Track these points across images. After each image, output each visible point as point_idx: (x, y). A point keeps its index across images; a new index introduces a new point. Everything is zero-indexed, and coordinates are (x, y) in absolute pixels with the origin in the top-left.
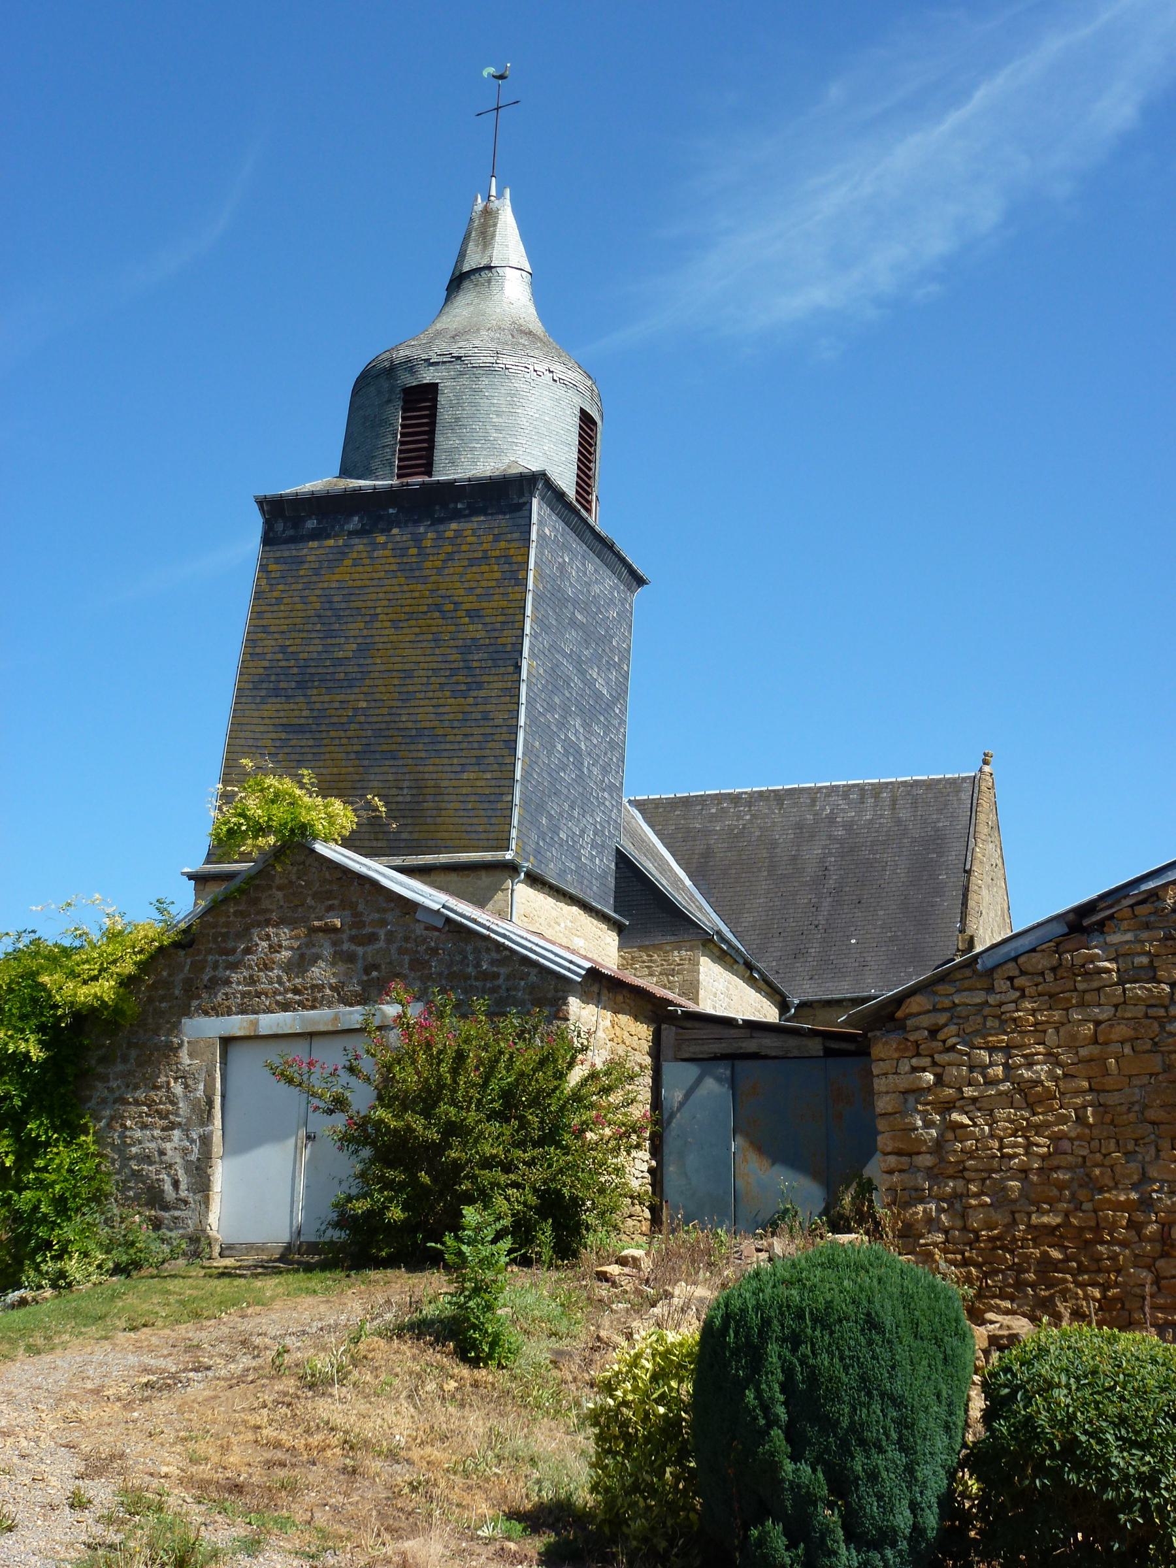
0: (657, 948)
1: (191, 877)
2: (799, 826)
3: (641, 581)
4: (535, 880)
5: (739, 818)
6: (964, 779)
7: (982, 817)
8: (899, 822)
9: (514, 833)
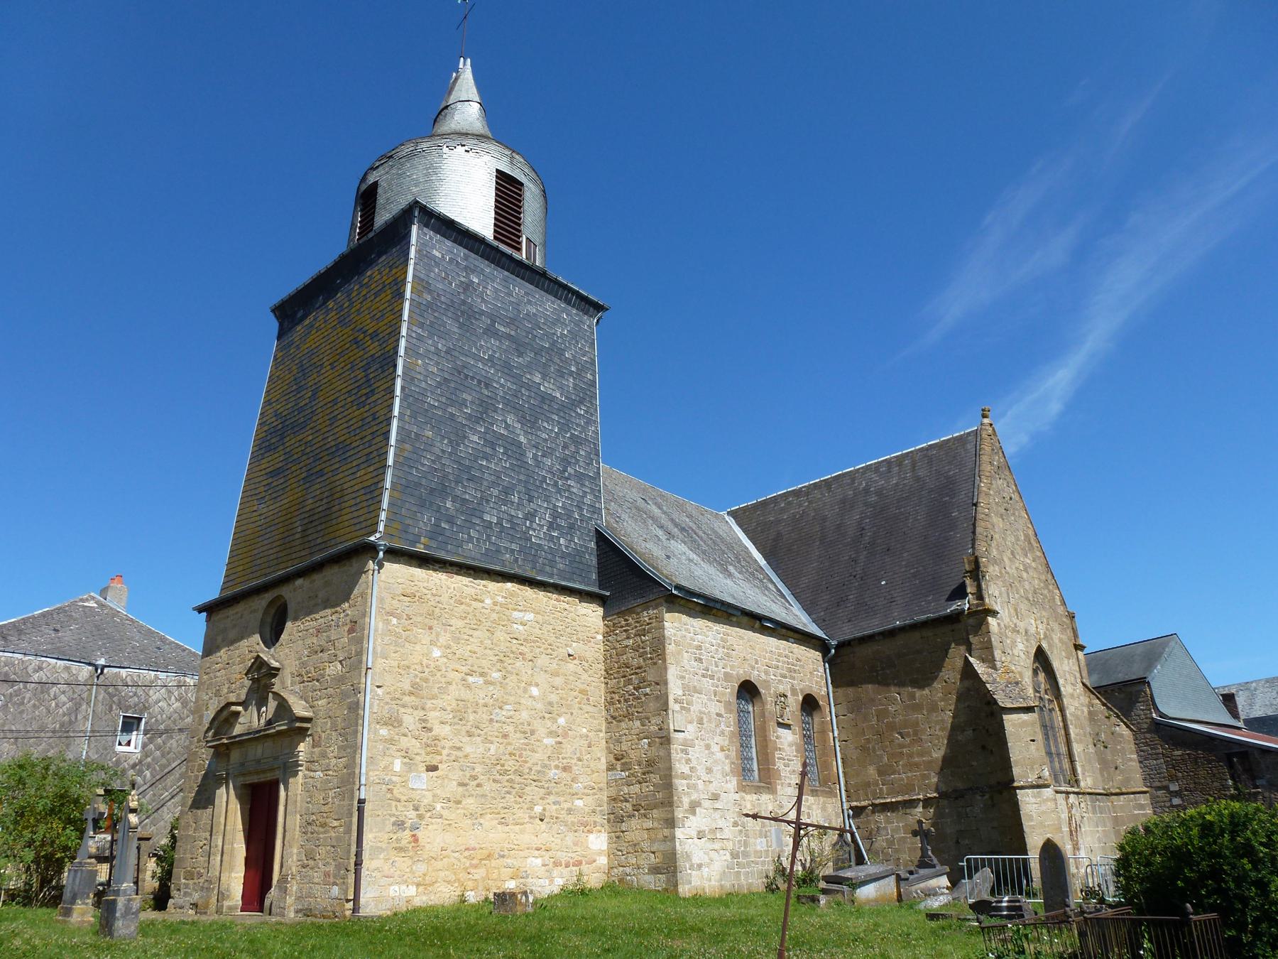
0: (630, 611)
1: (200, 610)
2: (843, 501)
3: (598, 308)
4: (395, 554)
5: (800, 505)
6: (969, 434)
7: (985, 458)
8: (918, 479)
9: (383, 516)
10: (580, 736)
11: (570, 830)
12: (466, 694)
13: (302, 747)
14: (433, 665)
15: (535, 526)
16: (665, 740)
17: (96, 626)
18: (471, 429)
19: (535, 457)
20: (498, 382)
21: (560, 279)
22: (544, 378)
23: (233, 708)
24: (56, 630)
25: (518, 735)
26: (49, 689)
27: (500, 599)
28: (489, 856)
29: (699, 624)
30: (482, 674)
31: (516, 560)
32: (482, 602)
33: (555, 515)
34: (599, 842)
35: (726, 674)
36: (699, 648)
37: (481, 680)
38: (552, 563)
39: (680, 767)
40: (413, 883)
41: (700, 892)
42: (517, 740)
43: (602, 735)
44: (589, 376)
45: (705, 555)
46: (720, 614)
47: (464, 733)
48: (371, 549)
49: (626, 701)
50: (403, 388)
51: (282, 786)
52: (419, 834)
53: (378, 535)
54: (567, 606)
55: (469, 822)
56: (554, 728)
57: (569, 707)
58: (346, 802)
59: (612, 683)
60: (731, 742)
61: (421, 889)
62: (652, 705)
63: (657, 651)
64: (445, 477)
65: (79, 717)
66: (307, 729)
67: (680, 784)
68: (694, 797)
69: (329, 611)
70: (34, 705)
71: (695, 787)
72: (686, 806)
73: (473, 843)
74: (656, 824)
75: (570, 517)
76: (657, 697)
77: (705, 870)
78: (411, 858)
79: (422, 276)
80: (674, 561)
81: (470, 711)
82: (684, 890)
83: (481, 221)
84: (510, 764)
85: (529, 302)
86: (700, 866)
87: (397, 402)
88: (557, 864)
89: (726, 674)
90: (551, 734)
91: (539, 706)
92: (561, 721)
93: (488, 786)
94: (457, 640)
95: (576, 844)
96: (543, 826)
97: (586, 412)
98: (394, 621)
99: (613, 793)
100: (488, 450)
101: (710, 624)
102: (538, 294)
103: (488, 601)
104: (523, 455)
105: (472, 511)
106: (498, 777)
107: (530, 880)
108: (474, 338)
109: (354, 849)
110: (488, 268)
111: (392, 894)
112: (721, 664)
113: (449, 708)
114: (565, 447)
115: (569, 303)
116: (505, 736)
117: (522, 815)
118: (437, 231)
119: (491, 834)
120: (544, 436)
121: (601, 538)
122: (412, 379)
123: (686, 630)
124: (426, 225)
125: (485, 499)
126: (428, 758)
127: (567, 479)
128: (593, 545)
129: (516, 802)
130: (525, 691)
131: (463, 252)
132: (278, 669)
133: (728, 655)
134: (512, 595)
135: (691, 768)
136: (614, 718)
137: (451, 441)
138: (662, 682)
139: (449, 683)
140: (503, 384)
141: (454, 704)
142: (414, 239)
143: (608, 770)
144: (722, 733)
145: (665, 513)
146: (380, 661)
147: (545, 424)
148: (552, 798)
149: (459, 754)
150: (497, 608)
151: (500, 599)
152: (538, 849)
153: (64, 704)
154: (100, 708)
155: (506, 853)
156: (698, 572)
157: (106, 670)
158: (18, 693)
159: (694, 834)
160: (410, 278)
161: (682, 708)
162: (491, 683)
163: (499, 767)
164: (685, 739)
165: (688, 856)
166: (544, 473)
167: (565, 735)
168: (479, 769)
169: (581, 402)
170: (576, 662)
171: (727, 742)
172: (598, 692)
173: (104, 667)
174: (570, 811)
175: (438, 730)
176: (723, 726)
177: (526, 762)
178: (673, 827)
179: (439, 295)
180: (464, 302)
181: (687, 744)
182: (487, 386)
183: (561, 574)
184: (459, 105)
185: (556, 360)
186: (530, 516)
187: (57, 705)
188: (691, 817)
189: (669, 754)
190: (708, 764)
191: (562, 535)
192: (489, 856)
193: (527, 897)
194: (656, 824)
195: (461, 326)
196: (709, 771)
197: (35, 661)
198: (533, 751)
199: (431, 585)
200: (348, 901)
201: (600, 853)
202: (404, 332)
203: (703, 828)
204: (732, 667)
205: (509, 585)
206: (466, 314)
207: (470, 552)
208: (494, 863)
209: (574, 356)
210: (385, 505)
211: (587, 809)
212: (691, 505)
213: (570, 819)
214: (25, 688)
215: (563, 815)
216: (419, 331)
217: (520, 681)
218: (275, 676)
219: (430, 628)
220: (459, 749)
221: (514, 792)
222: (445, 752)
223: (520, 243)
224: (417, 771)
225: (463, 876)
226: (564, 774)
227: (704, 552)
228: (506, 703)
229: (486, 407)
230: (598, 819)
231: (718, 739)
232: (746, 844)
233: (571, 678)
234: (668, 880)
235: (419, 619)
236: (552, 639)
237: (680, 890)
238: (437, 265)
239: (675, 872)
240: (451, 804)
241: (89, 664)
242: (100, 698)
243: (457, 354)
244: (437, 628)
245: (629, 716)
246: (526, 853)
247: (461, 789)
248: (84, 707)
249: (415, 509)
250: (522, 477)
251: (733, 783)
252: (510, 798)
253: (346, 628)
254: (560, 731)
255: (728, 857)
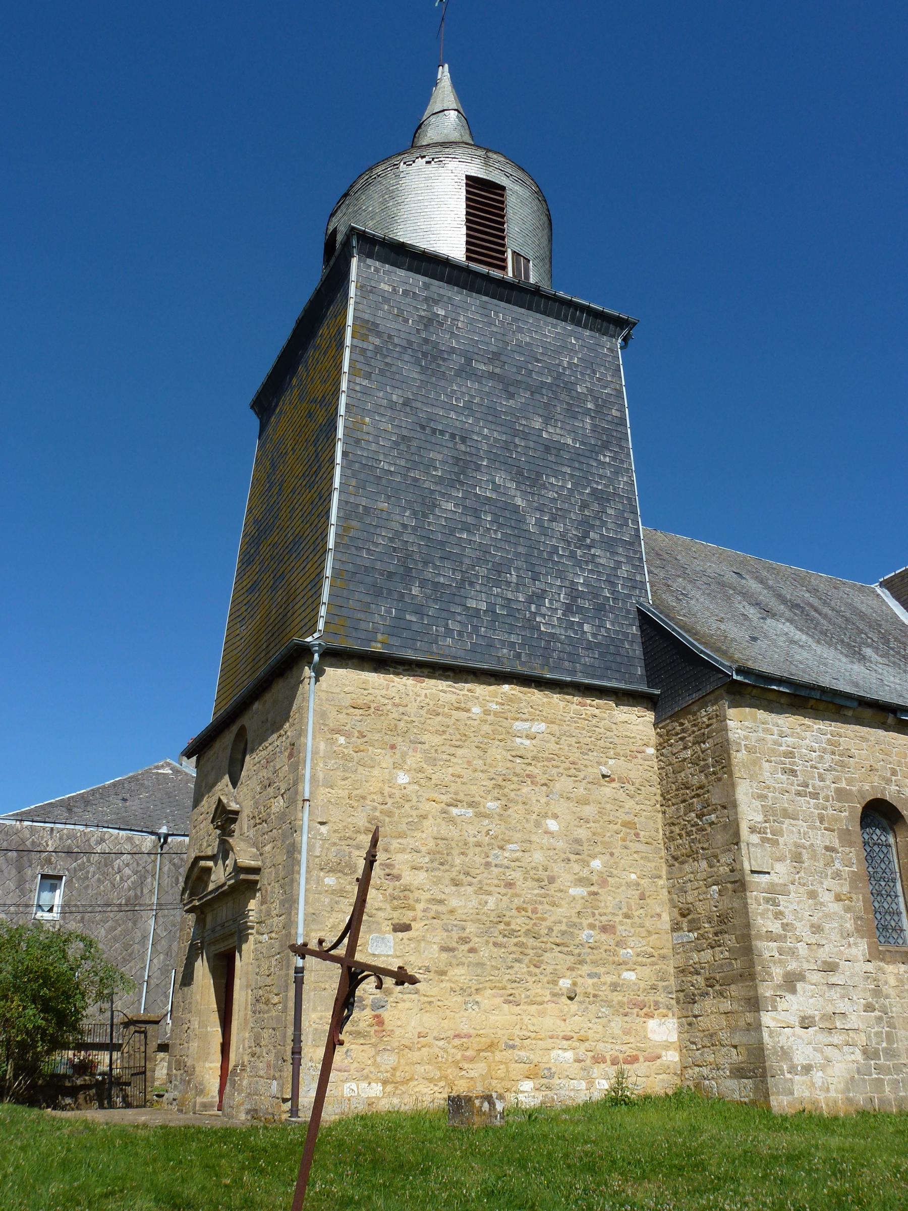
0: (685, 711)
3: (620, 323)
4: (337, 656)
9: (323, 611)
10: (633, 885)
11: (616, 1013)
12: (445, 830)
13: (253, 904)
14: (398, 794)
15: (543, 610)
16: (738, 885)
17: (167, 794)
18: (443, 495)
19: (539, 523)
20: (479, 434)
21: (561, 294)
22: (547, 420)
23: (202, 863)
24: (124, 800)
25: (529, 883)
26: (112, 862)
27: (494, 707)
28: (491, 1046)
29: (787, 722)
30: (471, 805)
31: (518, 656)
32: (468, 711)
33: (574, 593)
34: (664, 1030)
35: (839, 791)
36: (790, 755)
37: (470, 812)
38: (573, 657)
39: (764, 922)
40: (378, 1080)
41: (809, 1107)
42: (528, 890)
43: (661, 882)
44: (614, 412)
45: (825, 637)
46: (822, 706)
47: (447, 881)
48: (302, 653)
49: (689, 834)
50: (345, 454)
51: (237, 954)
52: (385, 1014)
53: (316, 635)
54: (597, 712)
55: (459, 999)
56: (585, 873)
57: (606, 845)
58: (283, 972)
59: (671, 811)
60: (853, 886)
61: (389, 1088)
62: (720, 838)
63: (720, 762)
64: (409, 556)
65: (146, 891)
66: (256, 882)
67: (766, 949)
68: (793, 966)
69: (275, 736)
70: (99, 880)
71: (793, 952)
72: (778, 978)
73: (465, 1029)
74: (735, 1007)
75: (597, 596)
76: (725, 827)
77: (818, 1076)
78: (374, 1046)
79: (366, 317)
80: (762, 644)
81: (455, 852)
82: (780, 1103)
83: (449, 239)
84: (519, 922)
85: (520, 330)
86: (807, 1069)
87: (338, 471)
88: (598, 1059)
89: (839, 791)
90: (580, 881)
91: (561, 844)
92: (596, 864)
93: (485, 953)
94: (433, 762)
95: (627, 1032)
96: (574, 1006)
97: (614, 459)
98: (342, 740)
99: (680, 961)
100: (470, 520)
101: (807, 721)
102: (531, 318)
103: (476, 710)
104: (522, 521)
105: (448, 598)
106: (500, 939)
107: (556, 1081)
108: (442, 383)
109: (290, 1031)
110: (457, 295)
111: (347, 1093)
112: (829, 777)
113: (424, 849)
114: (584, 506)
115: (578, 324)
116: (510, 885)
117: (541, 991)
118: (384, 260)
119: (493, 1016)
120: (551, 495)
121: (644, 619)
122: (358, 441)
123: (766, 731)
124: (370, 255)
125: (467, 581)
126: (395, 915)
127: (589, 547)
128: (634, 630)
129: (530, 974)
130: (538, 824)
131: (421, 280)
132: (237, 813)
133: (843, 765)
134: (511, 700)
135: (785, 926)
136: (675, 858)
137: (415, 513)
138: (730, 805)
139: (424, 817)
140: (486, 435)
141: (431, 844)
142: (353, 275)
143: (674, 930)
144: (837, 875)
145: (769, 588)
146: (323, 790)
147: (553, 480)
148: (585, 969)
149: (440, 908)
150: (491, 718)
151: (494, 707)
152: (551, 1037)
153: (129, 877)
154: (166, 881)
155: (517, 1042)
156: (801, 655)
157: (170, 839)
158: (82, 867)
159: (795, 1020)
160: (350, 321)
161: (764, 840)
162: (487, 816)
163: (502, 926)
164: (773, 884)
165: (785, 1054)
166: (554, 542)
167: (603, 883)
168: (471, 928)
169: (606, 446)
170: (615, 785)
171: (846, 889)
172: (653, 823)
173: (166, 836)
174: (615, 987)
175: (408, 877)
176: (838, 865)
177: (544, 919)
178: (758, 1010)
179: (390, 336)
180: (426, 341)
181: (774, 893)
182: (464, 439)
183: (589, 670)
184: (433, 119)
185: (563, 396)
186: (537, 598)
187: (121, 879)
188: (789, 996)
189: (745, 905)
190: (815, 920)
191: (585, 620)
192: (491, 1046)
193: (492, 1104)
194: (735, 1007)
195: (423, 370)
196: (817, 929)
197: (97, 832)
198: (554, 904)
199: (392, 692)
200: (285, 1100)
201: (667, 1046)
202: (344, 386)
203: (810, 1012)
204: (850, 781)
205: (506, 687)
206: (430, 357)
207: (449, 649)
208: (498, 1056)
209: (590, 390)
210: (325, 598)
211: (642, 985)
212: (821, 579)
213: (617, 997)
214: (89, 861)
215: (605, 991)
216: (365, 382)
217: (529, 812)
218: (234, 821)
219: (393, 747)
220: (441, 902)
221: (526, 960)
222: (420, 906)
223: (504, 260)
224: (379, 931)
225: (451, 1072)
226: (604, 937)
227: (824, 633)
228: (509, 842)
229: (463, 468)
230: (662, 998)
231: (828, 883)
232: (890, 1038)
233: (609, 807)
234: (756, 1089)
235: (377, 736)
236: (575, 755)
237: (774, 1101)
238: (386, 300)
239: (764, 1076)
240: (431, 975)
241: (152, 833)
242: (166, 869)
243: (419, 405)
244: (402, 746)
245: (692, 855)
246: (548, 1043)
247: (444, 955)
248: (149, 880)
249: (368, 599)
250: (521, 550)
251: (861, 948)
252: (521, 969)
253: (286, 754)
254: (594, 878)
255: (859, 1056)
